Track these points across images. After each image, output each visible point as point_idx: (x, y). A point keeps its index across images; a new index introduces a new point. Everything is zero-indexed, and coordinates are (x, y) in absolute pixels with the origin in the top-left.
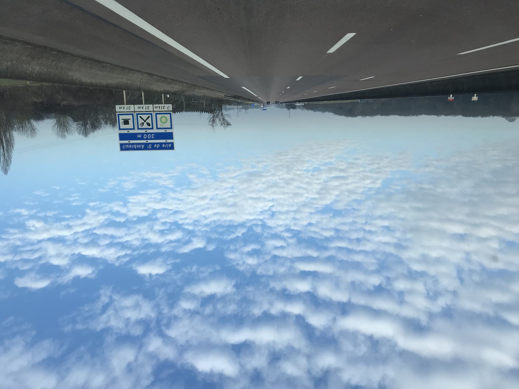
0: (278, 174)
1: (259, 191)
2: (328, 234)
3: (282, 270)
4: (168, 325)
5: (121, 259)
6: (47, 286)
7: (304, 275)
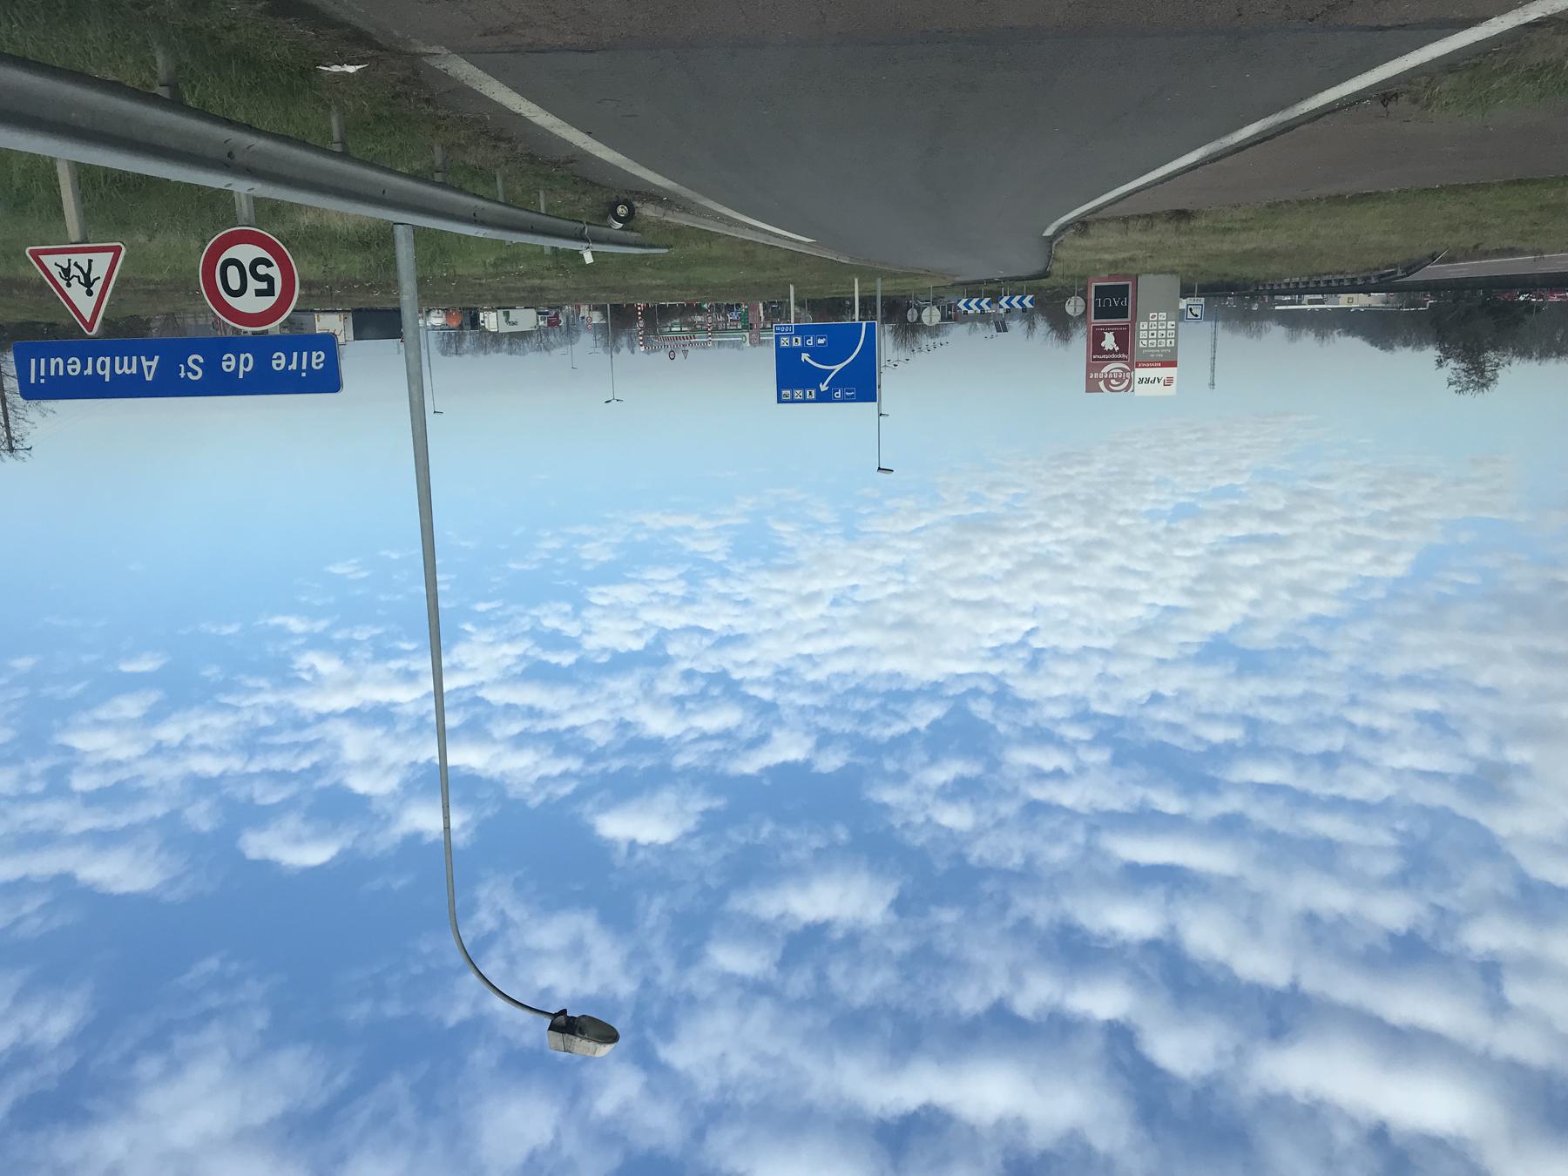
0: (1056, 524)
1: (985, 580)
2: (1218, 734)
3: (1058, 854)
4: (667, 1028)
5: (550, 788)
6: (333, 859)
7: (1140, 878)
